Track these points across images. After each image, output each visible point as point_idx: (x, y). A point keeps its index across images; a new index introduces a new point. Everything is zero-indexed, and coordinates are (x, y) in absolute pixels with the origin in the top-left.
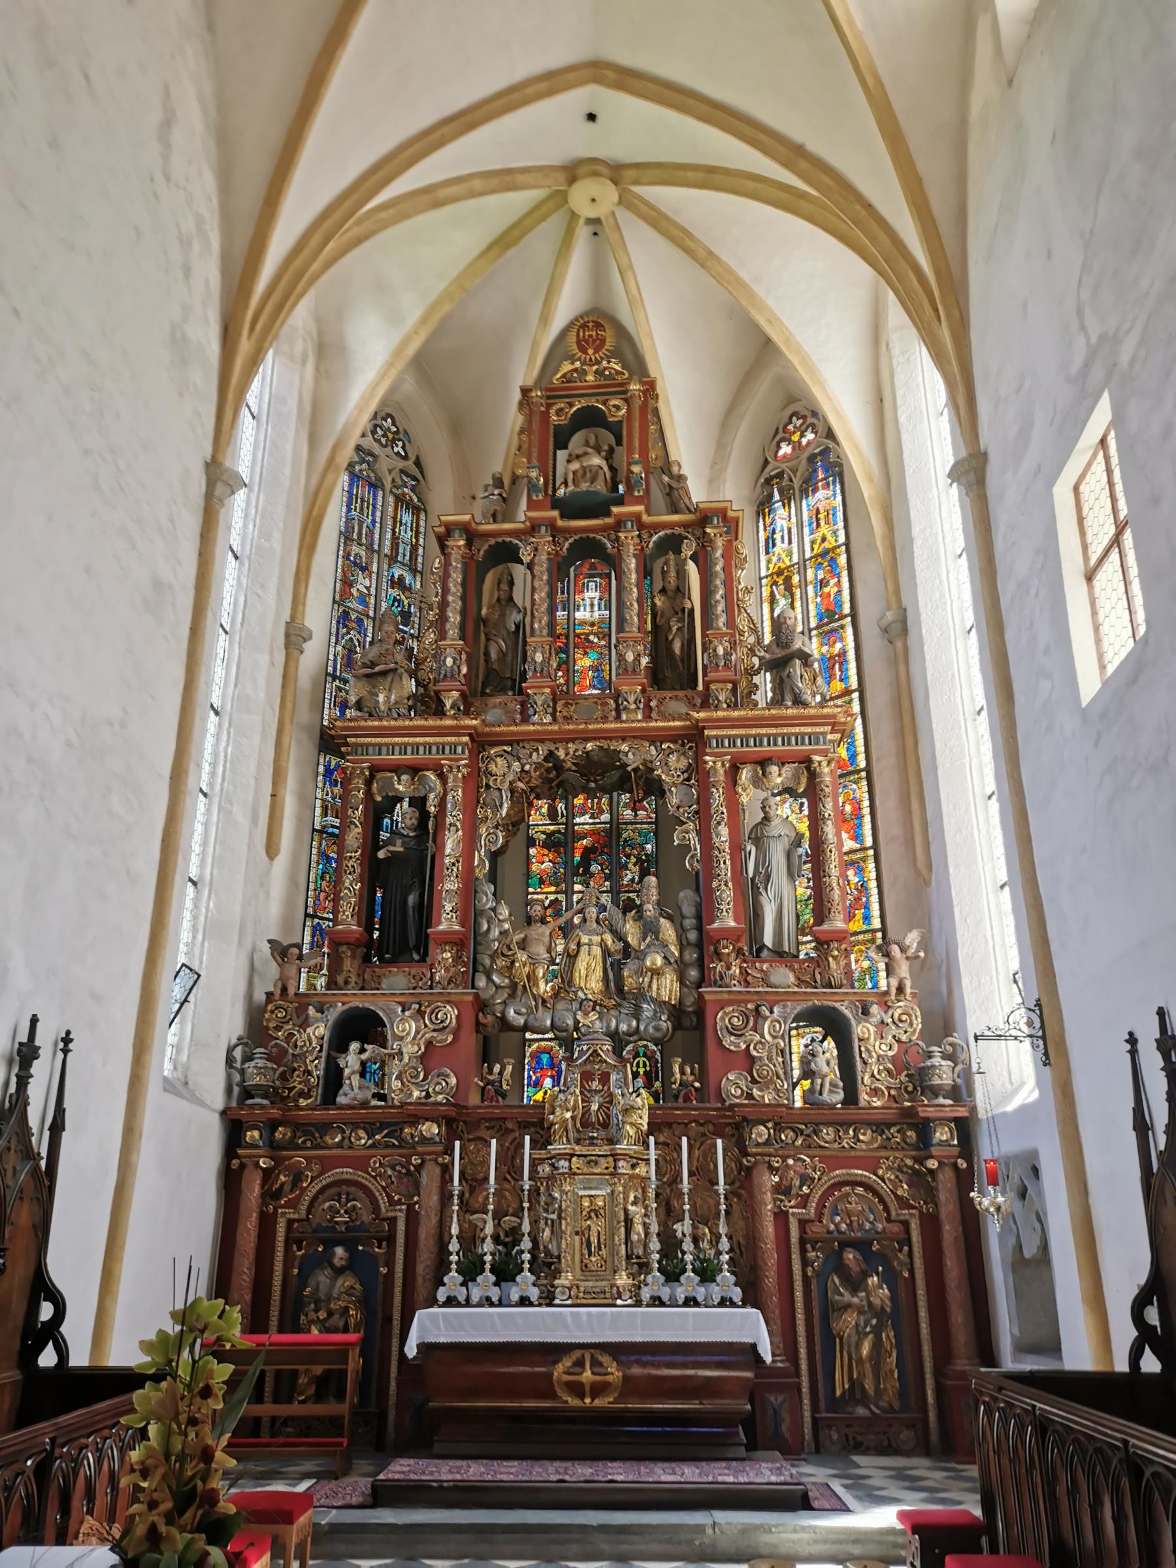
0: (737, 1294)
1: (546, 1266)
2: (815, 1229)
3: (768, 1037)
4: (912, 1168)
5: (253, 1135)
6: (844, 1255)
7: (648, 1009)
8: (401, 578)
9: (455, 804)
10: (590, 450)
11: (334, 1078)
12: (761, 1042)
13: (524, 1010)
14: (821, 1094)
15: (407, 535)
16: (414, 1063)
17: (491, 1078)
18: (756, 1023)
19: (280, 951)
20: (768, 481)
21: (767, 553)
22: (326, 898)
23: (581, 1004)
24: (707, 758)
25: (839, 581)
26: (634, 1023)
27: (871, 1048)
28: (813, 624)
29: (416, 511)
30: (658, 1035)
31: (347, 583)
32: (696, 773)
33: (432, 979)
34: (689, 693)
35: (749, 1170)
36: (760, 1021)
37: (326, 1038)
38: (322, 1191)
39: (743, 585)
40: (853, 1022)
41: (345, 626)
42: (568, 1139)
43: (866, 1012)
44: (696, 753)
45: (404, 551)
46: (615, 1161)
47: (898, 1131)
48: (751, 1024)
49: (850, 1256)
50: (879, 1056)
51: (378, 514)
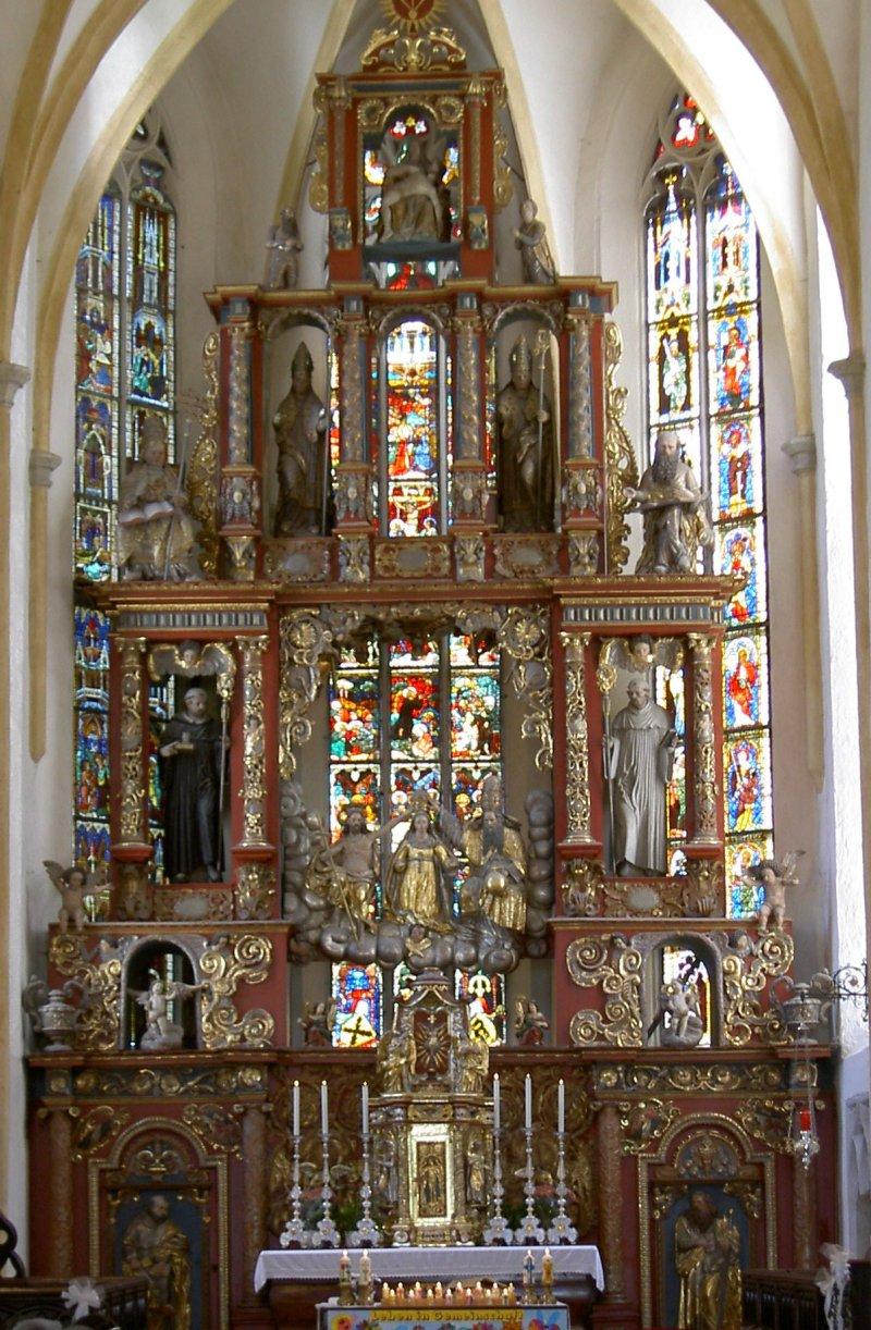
0: (572, 1234)
1: (386, 1213)
2: (664, 1174)
3: (623, 972)
4: (772, 1109)
5: (58, 1085)
6: (698, 1196)
7: (488, 937)
8: (149, 327)
9: (254, 690)
10: (414, 169)
11: (137, 1019)
12: (616, 979)
13: (343, 937)
14: (678, 1034)
15: (152, 260)
16: (225, 1003)
17: (315, 1018)
18: (609, 956)
19: (62, 877)
20: (662, 176)
21: (658, 287)
22: (88, 794)
23: (411, 930)
24: (563, 634)
25: (747, 355)
26: (473, 951)
27: (737, 984)
28: (714, 408)
29: (162, 217)
30: (502, 963)
31: (84, 356)
32: (550, 647)
33: (235, 901)
34: (544, 537)
35: (597, 1115)
36: (615, 955)
37: (123, 975)
38: (131, 1141)
39: (614, 386)
40: (719, 954)
41: (86, 420)
42: (402, 1087)
43: (733, 944)
44: (550, 620)
45: (151, 283)
46: (454, 1108)
47: (760, 1072)
48: (605, 958)
49: (699, 1198)
50: (744, 992)
51: (116, 238)
